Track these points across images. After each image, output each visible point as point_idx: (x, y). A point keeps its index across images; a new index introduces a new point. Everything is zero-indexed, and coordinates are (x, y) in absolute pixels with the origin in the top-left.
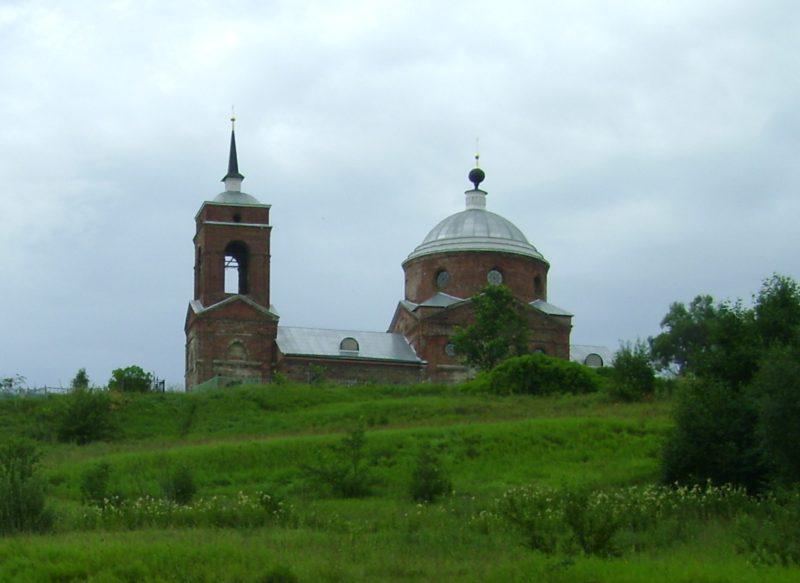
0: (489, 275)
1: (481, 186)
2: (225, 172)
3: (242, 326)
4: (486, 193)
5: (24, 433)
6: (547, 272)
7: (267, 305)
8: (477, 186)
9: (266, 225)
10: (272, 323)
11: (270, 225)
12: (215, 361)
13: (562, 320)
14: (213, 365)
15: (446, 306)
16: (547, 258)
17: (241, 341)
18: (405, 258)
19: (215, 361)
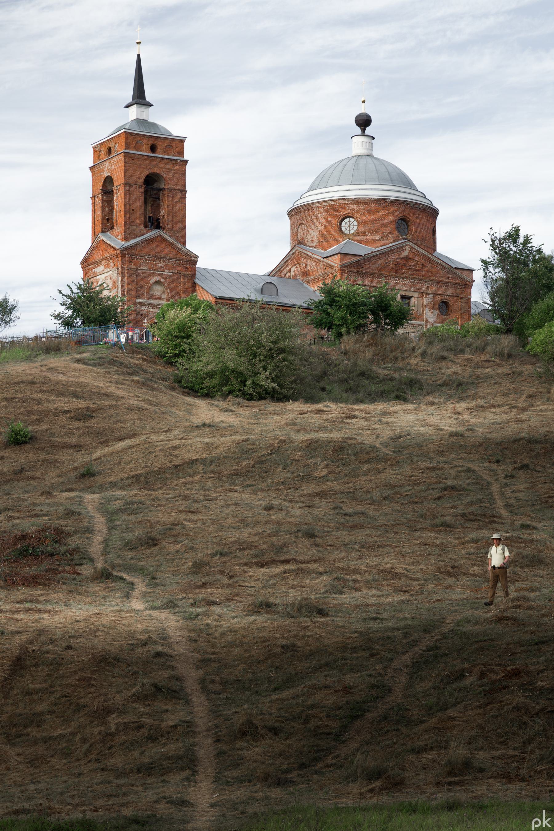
0: (352, 232)
1: (368, 131)
2: (130, 99)
3: (162, 265)
4: (373, 138)
5: (180, 636)
6: (436, 218)
7: (184, 244)
8: (363, 130)
9: (181, 158)
10: (192, 260)
11: (186, 158)
12: (138, 300)
13: (465, 275)
14: (136, 304)
15: (363, 254)
16: (436, 205)
17: (162, 280)
18: (289, 206)
19: (138, 300)
